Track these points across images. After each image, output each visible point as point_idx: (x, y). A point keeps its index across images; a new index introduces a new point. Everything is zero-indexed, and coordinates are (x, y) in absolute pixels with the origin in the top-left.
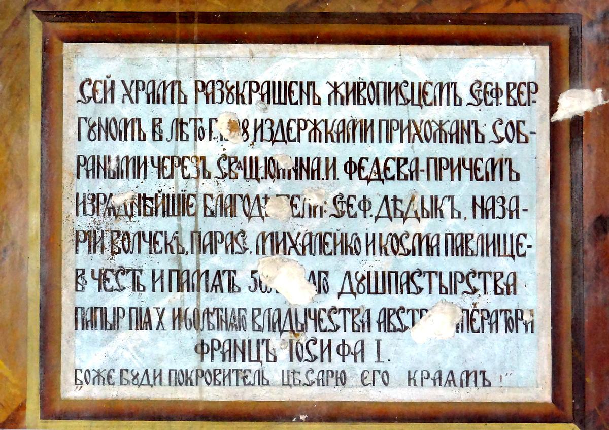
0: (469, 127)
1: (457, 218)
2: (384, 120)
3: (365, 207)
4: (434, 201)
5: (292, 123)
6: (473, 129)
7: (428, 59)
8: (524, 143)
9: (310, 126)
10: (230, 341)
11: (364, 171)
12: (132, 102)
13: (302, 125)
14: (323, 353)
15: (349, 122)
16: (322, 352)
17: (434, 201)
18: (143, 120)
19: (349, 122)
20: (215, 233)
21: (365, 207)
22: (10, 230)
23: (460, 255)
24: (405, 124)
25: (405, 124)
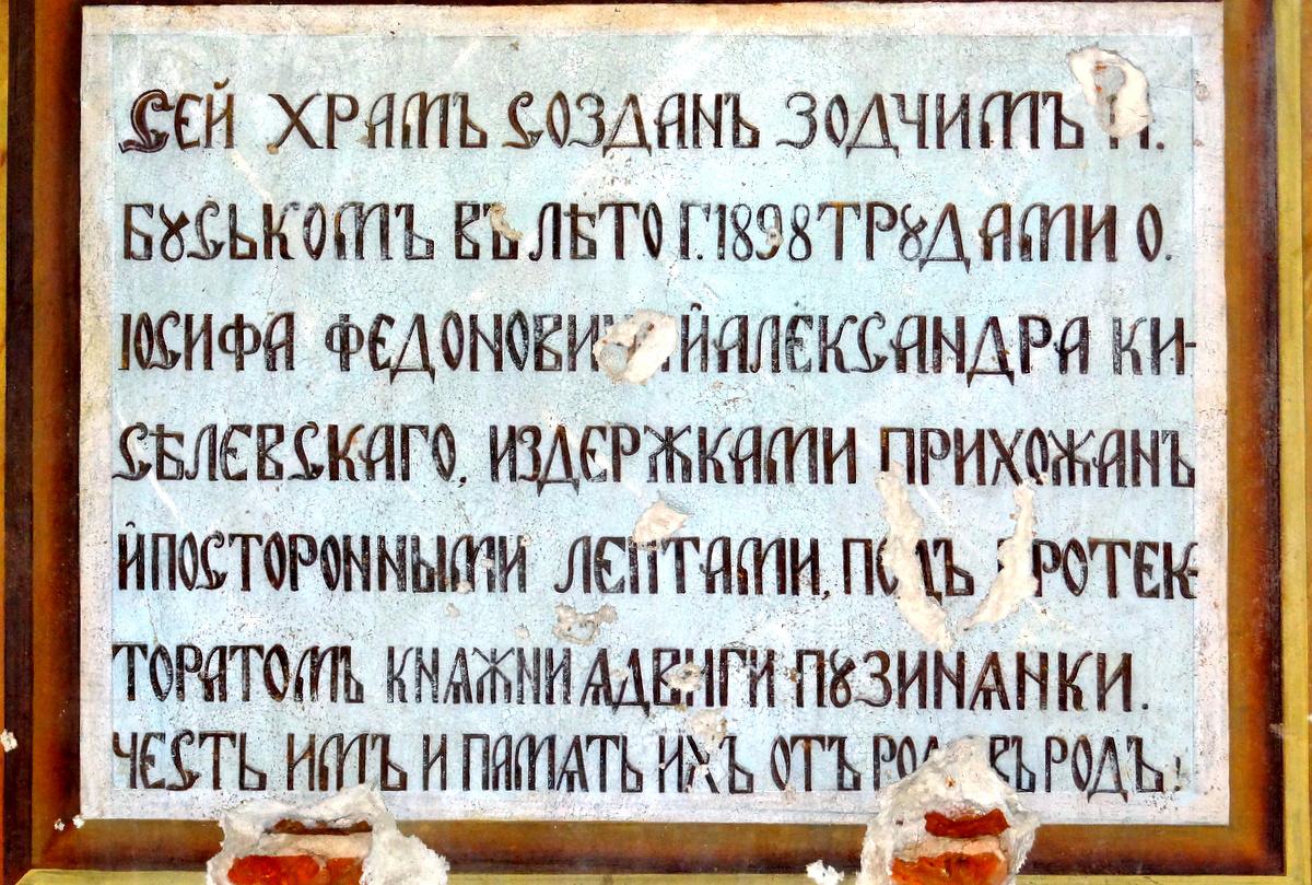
0: (1155, 449)
1: (413, 427)
2: (270, 427)
3: (240, 338)
4: (288, 557)
5: (595, 436)
6: (1165, 450)
7: (1302, 600)
8: (892, 430)
9: (650, 444)
10: (390, 430)
11: (609, 573)
12: (994, 433)
13: (626, 440)
14: (1106, 691)
15: (498, 742)
16: (190, 345)
17: (288, 557)
18: (463, 430)
19: (498, 742)
20: (405, 431)
21: (240, 338)
22: (976, 495)
23: (398, 477)
24: (969, 440)
25: (969, 440)
